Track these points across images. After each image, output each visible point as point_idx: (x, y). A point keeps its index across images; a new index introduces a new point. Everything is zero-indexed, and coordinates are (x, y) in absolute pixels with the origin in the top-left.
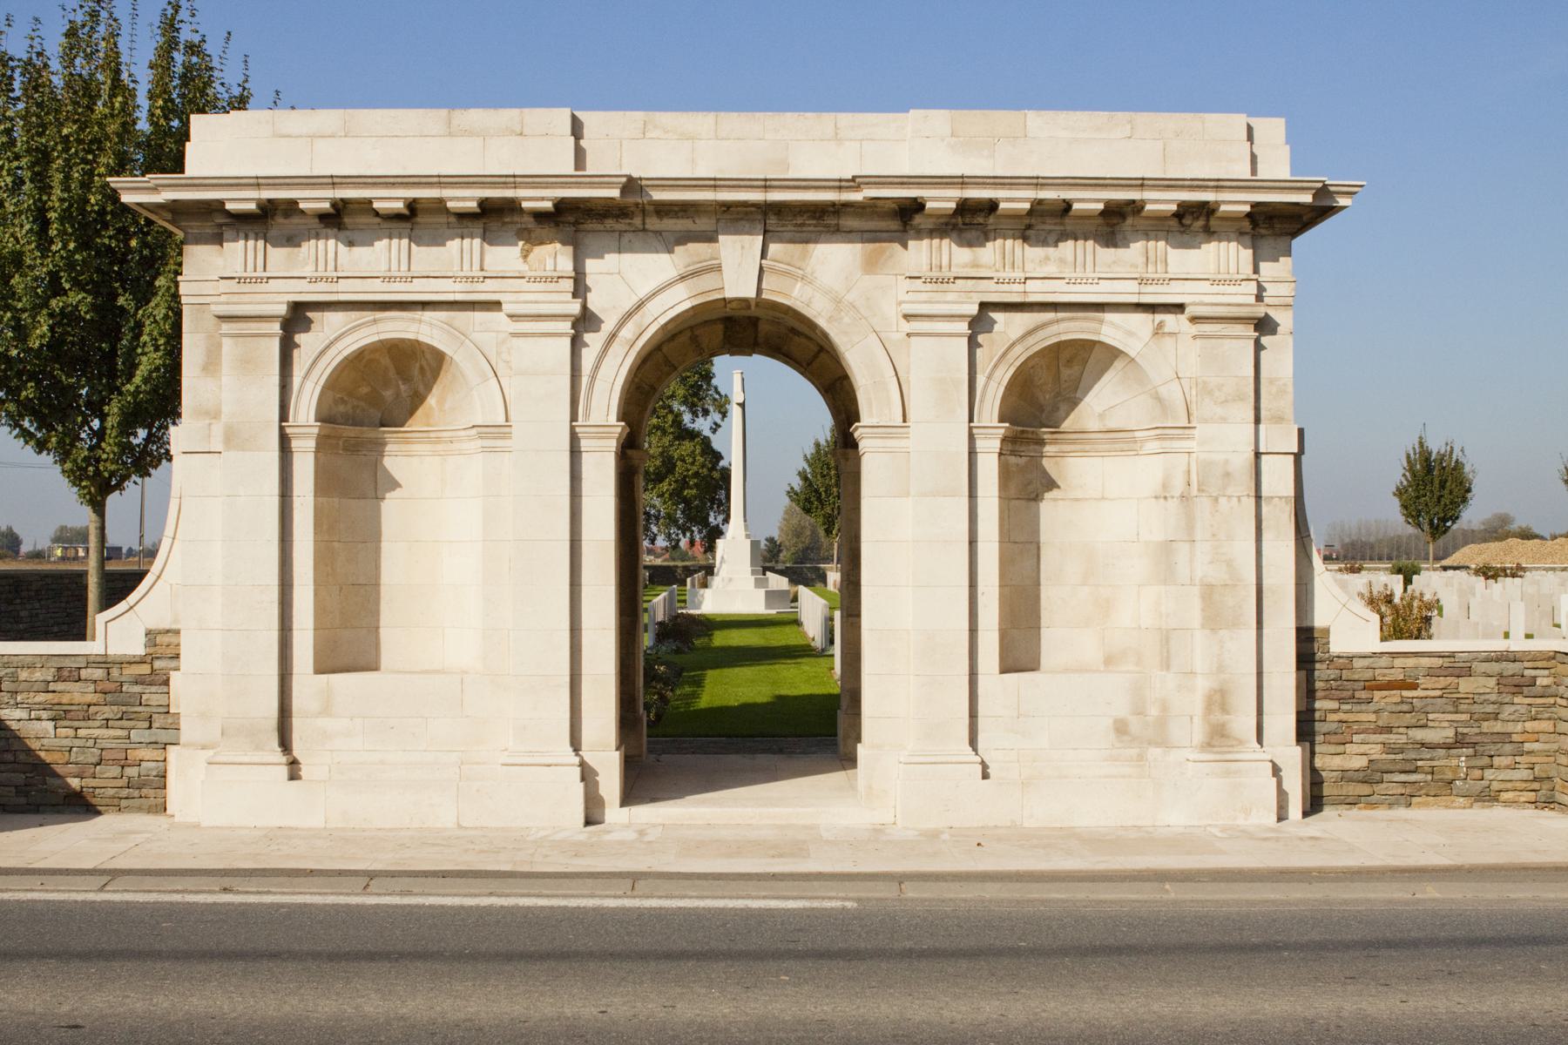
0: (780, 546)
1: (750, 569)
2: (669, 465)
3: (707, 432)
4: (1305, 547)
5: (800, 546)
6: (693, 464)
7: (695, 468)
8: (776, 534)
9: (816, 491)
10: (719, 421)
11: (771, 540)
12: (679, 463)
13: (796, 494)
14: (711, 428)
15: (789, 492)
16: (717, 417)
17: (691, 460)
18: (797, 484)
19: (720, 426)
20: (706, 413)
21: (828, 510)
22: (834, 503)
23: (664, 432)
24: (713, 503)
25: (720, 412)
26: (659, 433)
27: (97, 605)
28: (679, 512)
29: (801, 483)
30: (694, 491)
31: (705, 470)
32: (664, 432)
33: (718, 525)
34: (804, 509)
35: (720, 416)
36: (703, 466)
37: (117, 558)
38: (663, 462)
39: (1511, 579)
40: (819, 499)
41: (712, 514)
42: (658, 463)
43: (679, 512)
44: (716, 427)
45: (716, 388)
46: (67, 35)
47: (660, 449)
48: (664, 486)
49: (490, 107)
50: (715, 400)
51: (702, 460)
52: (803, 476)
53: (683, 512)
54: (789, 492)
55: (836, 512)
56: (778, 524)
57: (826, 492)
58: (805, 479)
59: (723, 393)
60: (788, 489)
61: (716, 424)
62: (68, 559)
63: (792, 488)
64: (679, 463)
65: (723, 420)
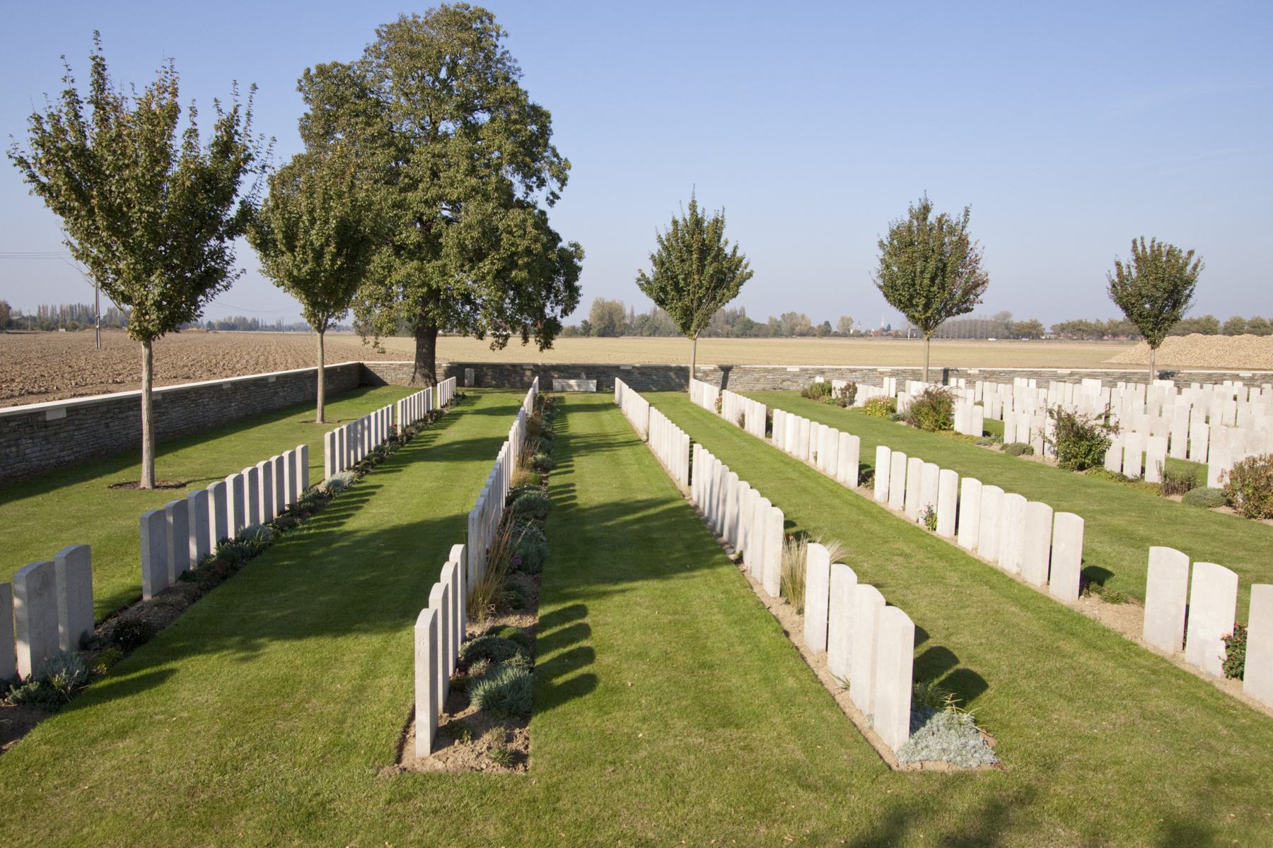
2: (491, 235)
3: (542, 205)
5: (603, 326)
7: (526, 243)
8: (587, 318)
9: (674, 278)
10: (557, 192)
11: (585, 322)
12: (504, 235)
13: (648, 282)
14: (547, 199)
15: (639, 280)
16: (553, 185)
17: (521, 232)
18: (650, 271)
19: (558, 198)
20: (542, 183)
21: (687, 301)
22: (694, 293)
23: (487, 197)
24: (549, 292)
25: (559, 179)
26: (479, 197)
28: (507, 301)
30: (524, 274)
31: (539, 245)
32: (487, 197)
35: (559, 185)
36: (536, 240)
41: (548, 304)
42: (475, 234)
43: (507, 301)
44: (553, 199)
45: (554, 150)
46: (567, 315)
47: (479, 217)
48: (486, 266)
49: (659, 465)
50: (552, 163)
51: (534, 232)
52: (659, 262)
53: (513, 301)
54: (639, 280)
55: (695, 304)
56: (1202, 316)
57: (684, 280)
59: (561, 156)
60: (639, 276)
61: (553, 194)
63: (643, 275)
64: (504, 235)
65: (561, 190)
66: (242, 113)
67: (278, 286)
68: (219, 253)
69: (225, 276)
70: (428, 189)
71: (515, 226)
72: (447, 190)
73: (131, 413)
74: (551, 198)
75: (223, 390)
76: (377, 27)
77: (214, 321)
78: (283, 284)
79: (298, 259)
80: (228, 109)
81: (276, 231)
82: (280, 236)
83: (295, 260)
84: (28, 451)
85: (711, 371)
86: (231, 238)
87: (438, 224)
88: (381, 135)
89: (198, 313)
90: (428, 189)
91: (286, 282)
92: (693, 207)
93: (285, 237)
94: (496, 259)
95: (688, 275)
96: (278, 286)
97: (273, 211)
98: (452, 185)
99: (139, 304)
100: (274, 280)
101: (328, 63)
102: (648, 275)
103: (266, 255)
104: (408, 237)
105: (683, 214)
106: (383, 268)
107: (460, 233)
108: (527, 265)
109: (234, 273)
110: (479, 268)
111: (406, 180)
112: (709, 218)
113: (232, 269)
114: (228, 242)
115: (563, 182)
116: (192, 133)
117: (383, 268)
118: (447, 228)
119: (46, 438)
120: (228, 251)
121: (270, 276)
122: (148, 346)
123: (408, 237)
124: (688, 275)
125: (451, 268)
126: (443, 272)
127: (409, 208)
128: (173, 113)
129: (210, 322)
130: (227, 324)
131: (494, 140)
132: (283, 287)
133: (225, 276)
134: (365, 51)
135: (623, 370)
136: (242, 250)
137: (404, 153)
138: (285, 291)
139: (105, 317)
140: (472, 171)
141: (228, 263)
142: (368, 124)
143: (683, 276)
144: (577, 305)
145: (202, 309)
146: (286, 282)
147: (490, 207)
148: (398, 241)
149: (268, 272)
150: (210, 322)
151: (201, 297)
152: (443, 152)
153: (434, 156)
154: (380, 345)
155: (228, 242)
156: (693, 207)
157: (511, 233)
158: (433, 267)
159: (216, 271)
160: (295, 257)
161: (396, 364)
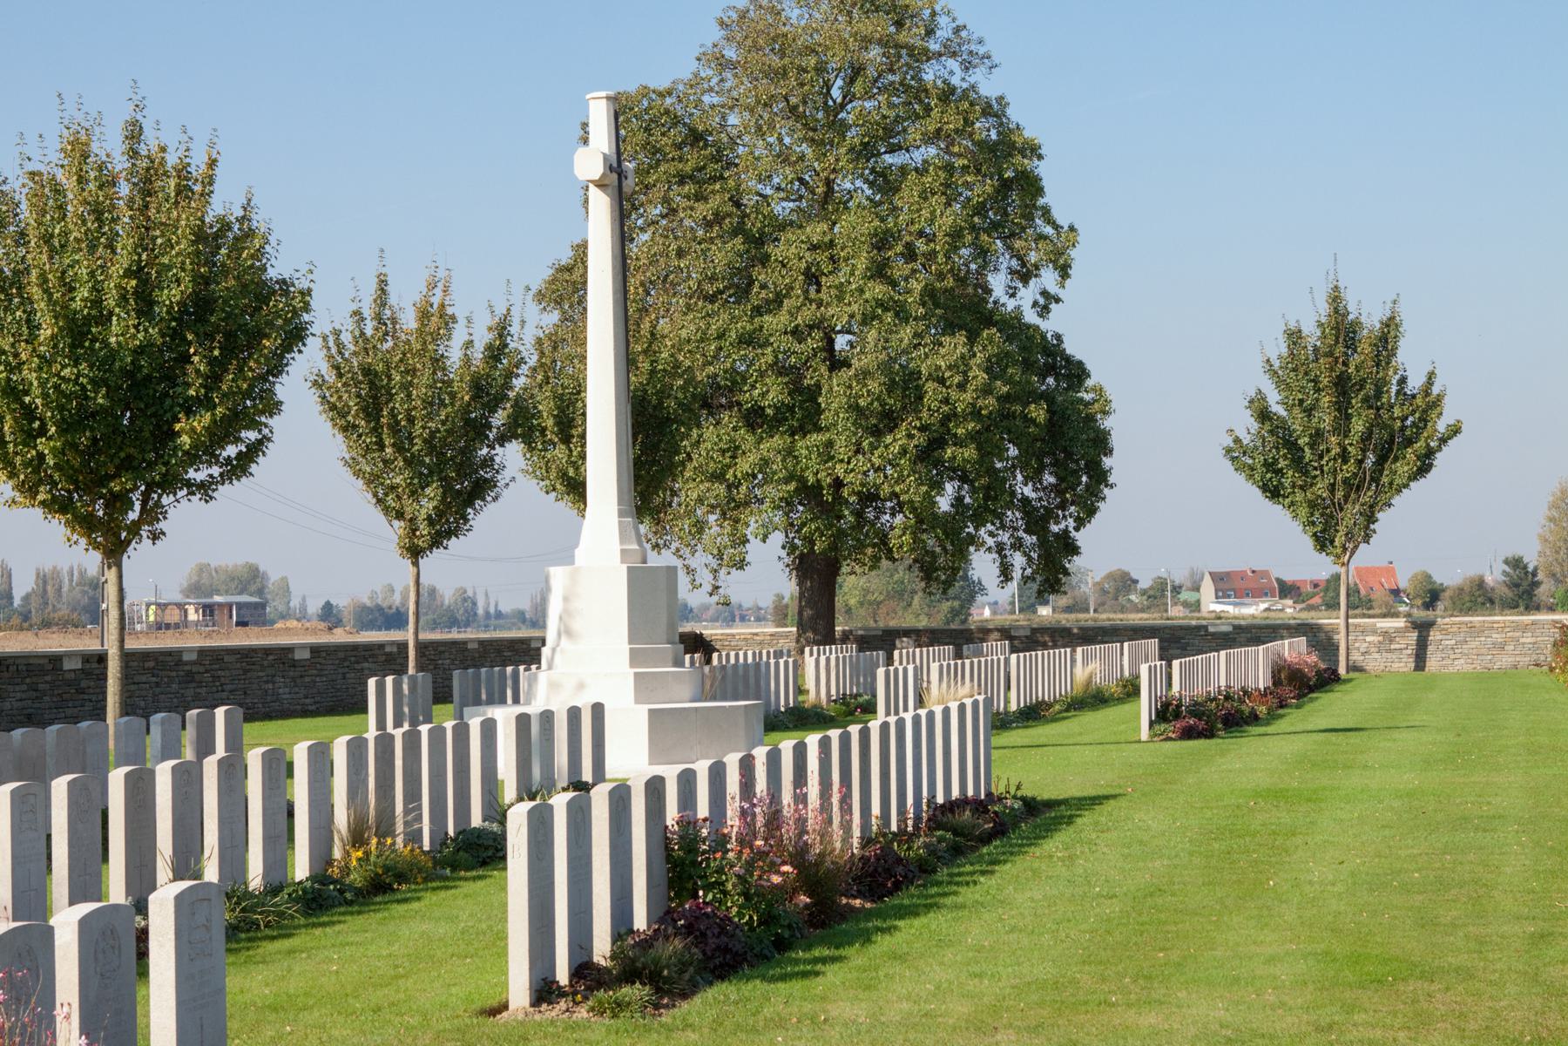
0: (1534, 574)
1: (626, 647)
2: (906, 385)
4: (490, 792)
6: (962, 387)
7: (968, 396)
9: (1292, 446)
10: (1053, 289)
11: (1516, 563)
15: (1229, 451)
16: (1048, 278)
18: (1246, 426)
19: (1058, 300)
27: (118, 711)
29: (1254, 426)
32: (902, 314)
33: (1066, 531)
34: (1264, 488)
37: (256, 624)
38: (891, 387)
39: (437, 553)
40: (1298, 462)
44: (1047, 302)
48: (896, 441)
54: (1229, 451)
57: (1312, 446)
58: (1264, 415)
59: (1063, 221)
60: (1229, 442)
61: (1045, 293)
62: (168, 626)
63: (1237, 440)
64: (930, 386)
66: (515, 313)
67: (547, 493)
68: (488, 462)
69: (495, 486)
70: (799, 308)
71: (950, 367)
72: (831, 311)
73: (366, 665)
74: (1042, 301)
75: (467, 649)
76: (720, 14)
77: (342, 602)
78: (554, 490)
79: (575, 453)
80: (501, 310)
81: (545, 414)
82: (550, 422)
83: (570, 456)
84: (281, 691)
85: (1398, 630)
86: (502, 445)
87: (815, 371)
88: (718, 218)
89: (467, 527)
90: (799, 308)
91: (558, 486)
92: (1336, 299)
93: (557, 424)
94: (915, 427)
95: (1317, 436)
96: (547, 493)
97: (541, 386)
98: (840, 298)
99: (411, 520)
100: (542, 483)
101: (631, 87)
102: (1246, 440)
103: (531, 449)
104: (763, 395)
105: (1311, 318)
106: (723, 452)
107: (850, 387)
108: (973, 437)
109: (503, 482)
110: (886, 447)
111: (763, 295)
112: (1370, 316)
113: (502, 479)
114: (498, 449)
115: (1064, 271)
116: (469, 344)
117: (723, 452)
118: (830, 377)
119: (294, 680)
120: (498, 459)
121: (536, 477)
122: (416, 564)
123: (763, 395)
124: (1317, 436)
125: (842, 449)
126: (827, 453)
127: (767, 344)
128: (448, 321)
129: (328, 606)
130: (379, 608)
131: (919, 210)
132: (554, 494)
133: (495, 486)
134: (699, 59)
135: (1213, 634)
136: (512, 456)
137: (758, 243)
138: (557, 500)
139: (26, 598)
140: (879, 271)
141: (498, 472)
142: (700, 197)
143: (1307, 440)
144: (1101, 505)
145: (471, 523)
146: (558, 486)
147: (906, 333)
148: (747, 402)
149: (534, 472)
150: (328, 606)
151: (469, 510)
152: (827, 239)
153: (814, 248)
154: (721, 591)
155: (498, 449)
156: (1336, 299)
157: (942, 381)
158: (807, 448)
159: (486, 480)
160: (571, 451)
161: (764, 634)
